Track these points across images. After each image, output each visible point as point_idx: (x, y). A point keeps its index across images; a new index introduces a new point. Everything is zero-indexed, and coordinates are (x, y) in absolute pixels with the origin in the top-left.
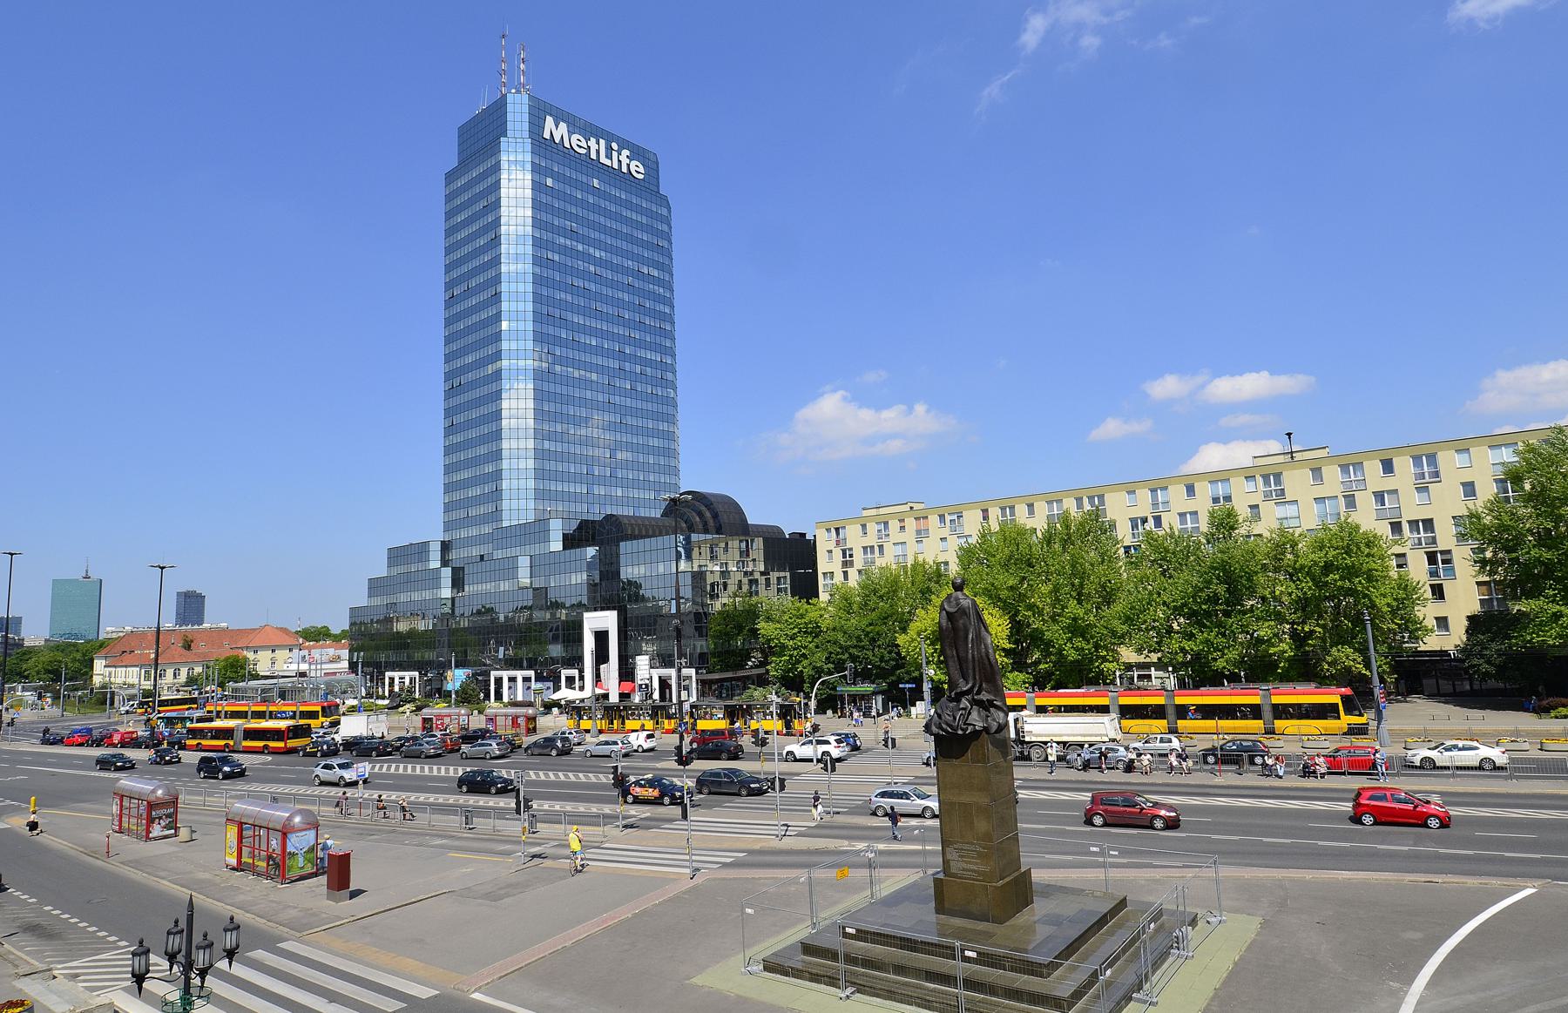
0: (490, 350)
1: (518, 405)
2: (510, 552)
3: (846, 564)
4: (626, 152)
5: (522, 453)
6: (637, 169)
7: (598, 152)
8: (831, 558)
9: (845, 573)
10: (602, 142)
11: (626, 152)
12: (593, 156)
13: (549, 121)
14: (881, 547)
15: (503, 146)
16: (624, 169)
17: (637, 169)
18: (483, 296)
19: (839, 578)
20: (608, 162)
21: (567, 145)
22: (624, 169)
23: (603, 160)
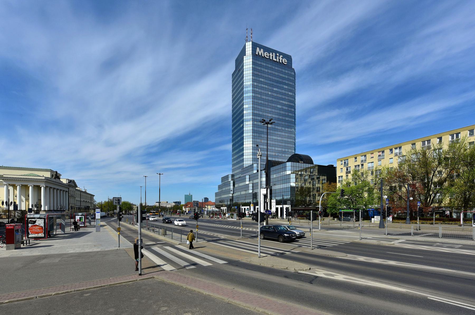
0: (241, 153)
1: (248, 144)
2: (245, 175)
3: (347, 173)
4: (281, 56)
5: (249, 154)
6: (285, 61)
7: (272, 57)
8: (342, 171)
9: (347, 176)
10: (274, 54)
11: (281, 56)
12: (271, 58)
13: (258, 49)
14: (362, 165)
15: (245, 59)
16: (281, 62)
17: (285, 61)
18: (239, 138)
19: (344, 177)
20: (276, 60)
21: (263, 56)
22: (281, 62)
23: (274, 59)
